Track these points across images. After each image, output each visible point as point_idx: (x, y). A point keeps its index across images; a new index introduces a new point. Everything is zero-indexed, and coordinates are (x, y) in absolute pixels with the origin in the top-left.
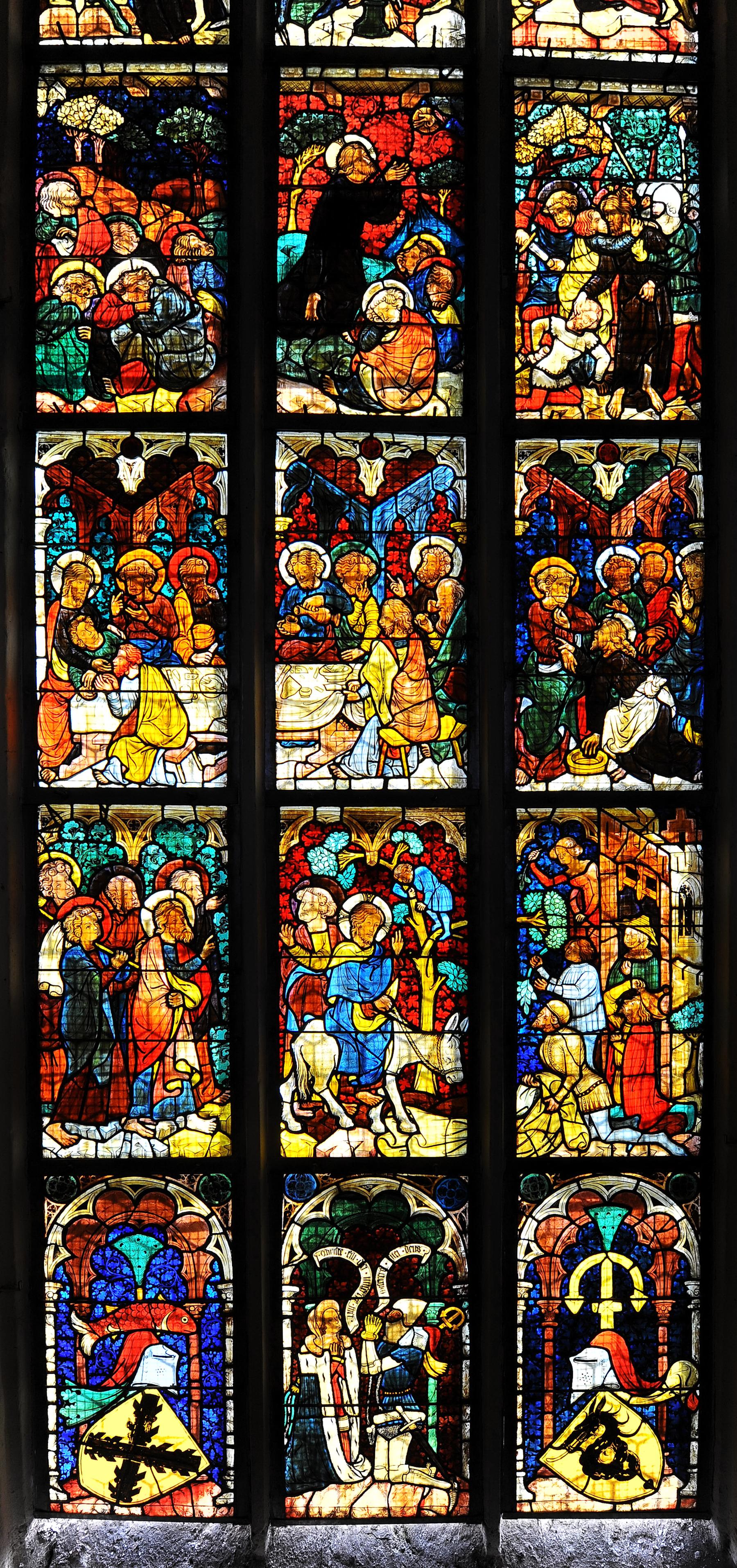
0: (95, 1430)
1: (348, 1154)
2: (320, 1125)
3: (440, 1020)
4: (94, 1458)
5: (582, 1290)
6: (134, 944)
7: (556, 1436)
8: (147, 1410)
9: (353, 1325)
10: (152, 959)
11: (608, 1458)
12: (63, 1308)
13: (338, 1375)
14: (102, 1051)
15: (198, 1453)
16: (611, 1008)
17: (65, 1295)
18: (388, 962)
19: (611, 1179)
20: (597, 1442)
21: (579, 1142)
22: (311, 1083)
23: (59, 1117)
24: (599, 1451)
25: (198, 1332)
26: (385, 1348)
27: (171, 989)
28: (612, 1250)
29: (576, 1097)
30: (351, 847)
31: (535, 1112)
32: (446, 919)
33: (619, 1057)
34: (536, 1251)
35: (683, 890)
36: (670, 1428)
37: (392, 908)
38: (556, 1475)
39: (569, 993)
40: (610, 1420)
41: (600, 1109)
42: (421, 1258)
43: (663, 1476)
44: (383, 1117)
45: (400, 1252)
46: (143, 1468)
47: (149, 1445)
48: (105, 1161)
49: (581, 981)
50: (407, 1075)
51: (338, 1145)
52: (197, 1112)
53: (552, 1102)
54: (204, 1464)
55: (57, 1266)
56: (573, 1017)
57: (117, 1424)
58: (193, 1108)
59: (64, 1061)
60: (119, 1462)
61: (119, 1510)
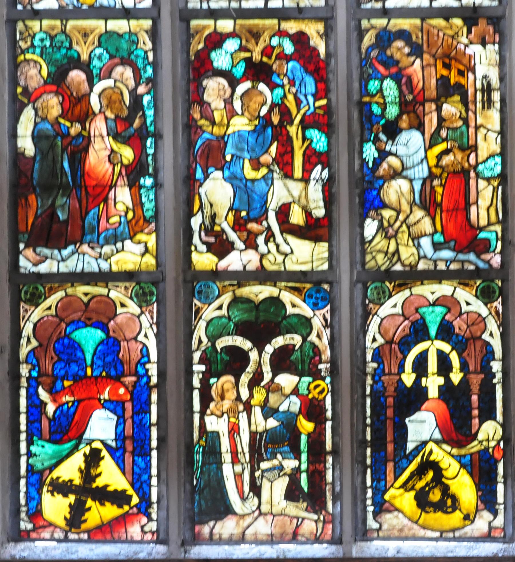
0: (55, 474)
1: (241, 268)
2: (221, 247)
3: (307, 171)
4: (53, 495)
5: (415, 369)
6: (85, 116)
7: (396, 479)
8: (93, 458)
9: (245, 394)
10: (99, 126)
11: (435, 498)
12: (33, 383)
13: (234, 430)
14: (63, 196)
15: (130, 491)
16: (433, 162)
17: (34, 374)
18: (269, 130)
19: (435, 287)
20: (427, 484)
21: (412, 260)
22: (213, 217)
23: (31, 244)
24: (428, 492)
25: (132, 399)
26: (269, 412)
27: (112, 151)
28: (436, 338)
29: (408, 227)
30: (242, 48)
31: (378, 238)
32: (311, 99)
33: (439, 198)
34: (380, 340)
35: (485, 77)
36: (482, 470)
37: (272, 92)
38: (396, 509)
39: (401, 151)
40: (435, 466)
41: (426, 235)
42: (294, 346)
43: (477, 510)
44: (266, 242)
45: (279, 341)
46: (90, 503)
47: (94, 485)
48: (63, 274)
49: (410, 144)
50: (283, 212)
51: (234, 261)
52: (131, 238)
53: (391, 231)
54: (135, 500)
55: (29, 352)
56: (404, 168)
57: (70, 470)
58: (128, 236)
59: (35, 204)
60: (72, 498)
61: (72, 536)
